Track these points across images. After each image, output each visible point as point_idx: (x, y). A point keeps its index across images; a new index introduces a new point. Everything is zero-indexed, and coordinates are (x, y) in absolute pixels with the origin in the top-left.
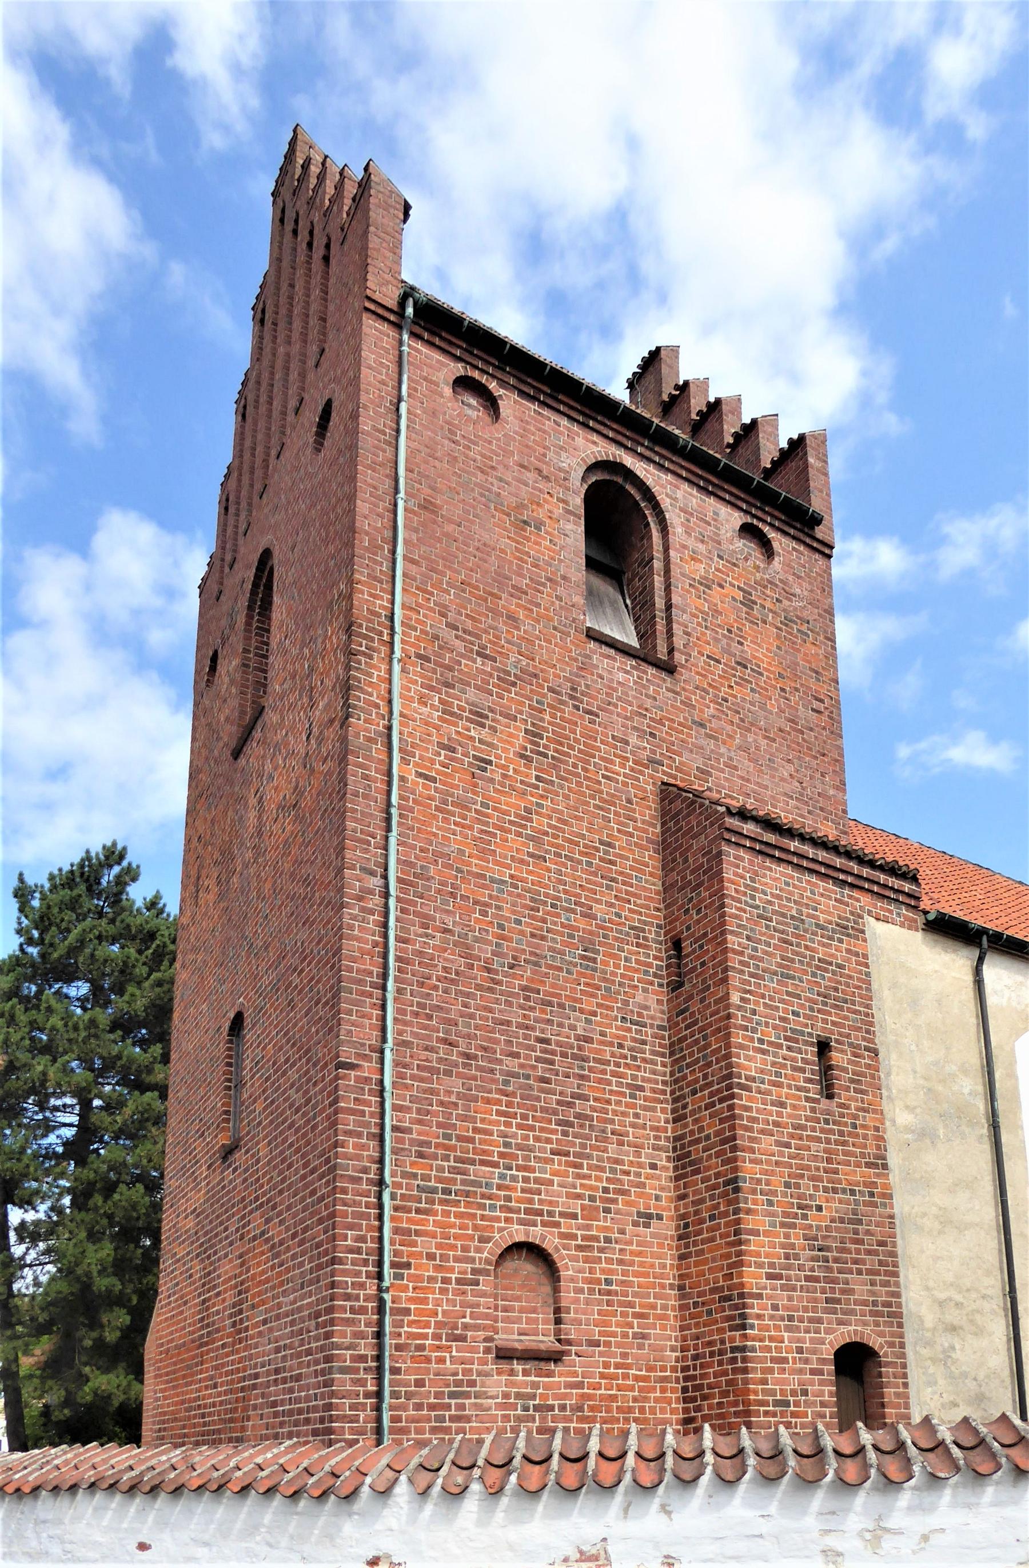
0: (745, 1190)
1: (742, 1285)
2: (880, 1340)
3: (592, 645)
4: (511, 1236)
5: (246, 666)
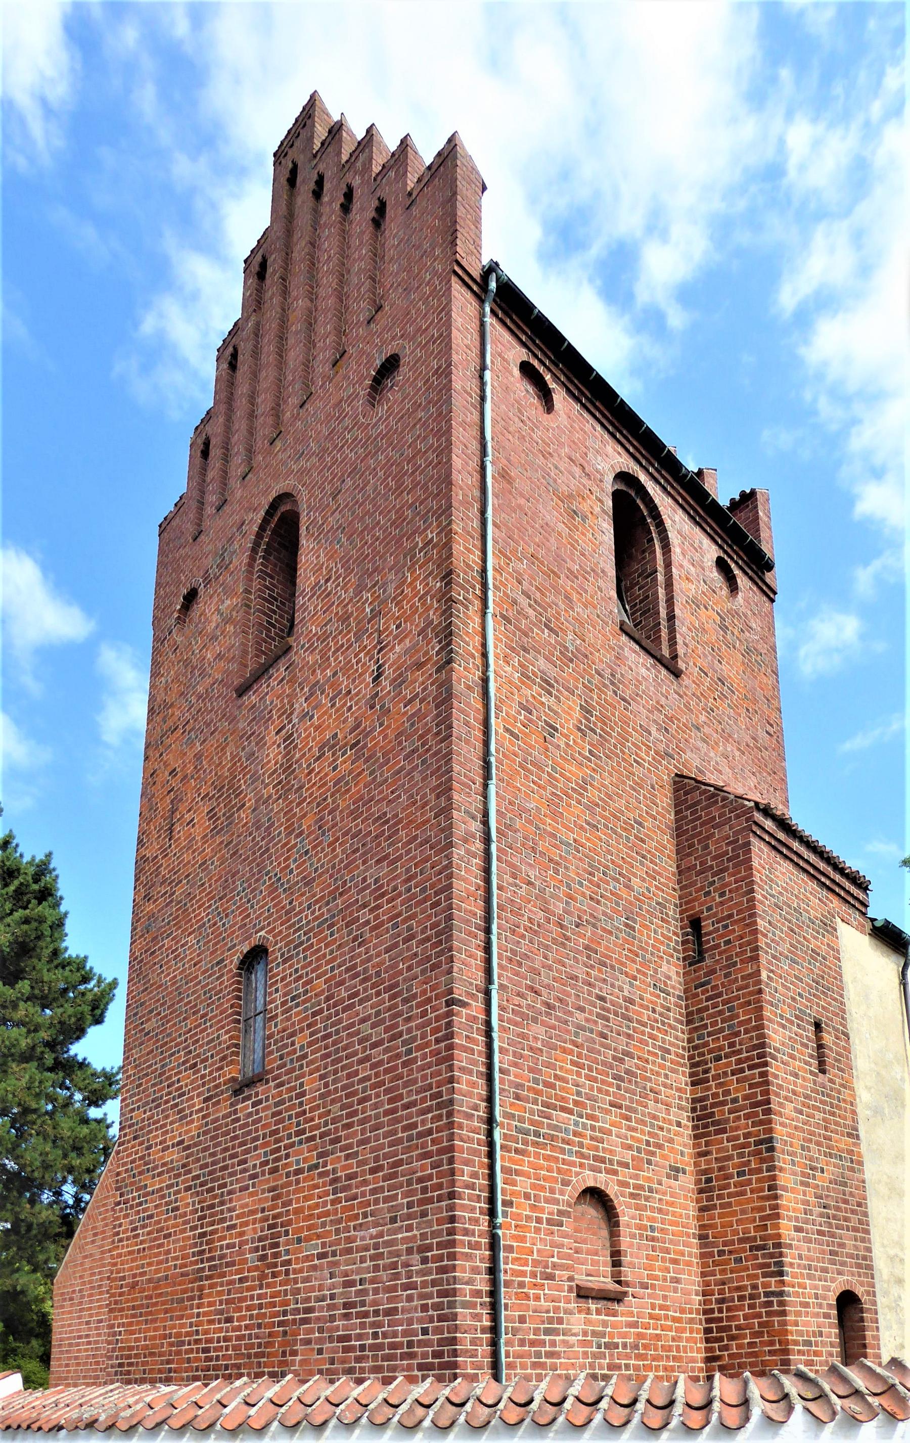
0: (778, 1150)
1: (779, 1236)
2: (862, 1289)
3: (624, 638)
5: (249, 607)
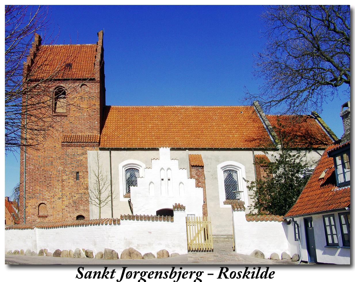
4: (38, 203)
